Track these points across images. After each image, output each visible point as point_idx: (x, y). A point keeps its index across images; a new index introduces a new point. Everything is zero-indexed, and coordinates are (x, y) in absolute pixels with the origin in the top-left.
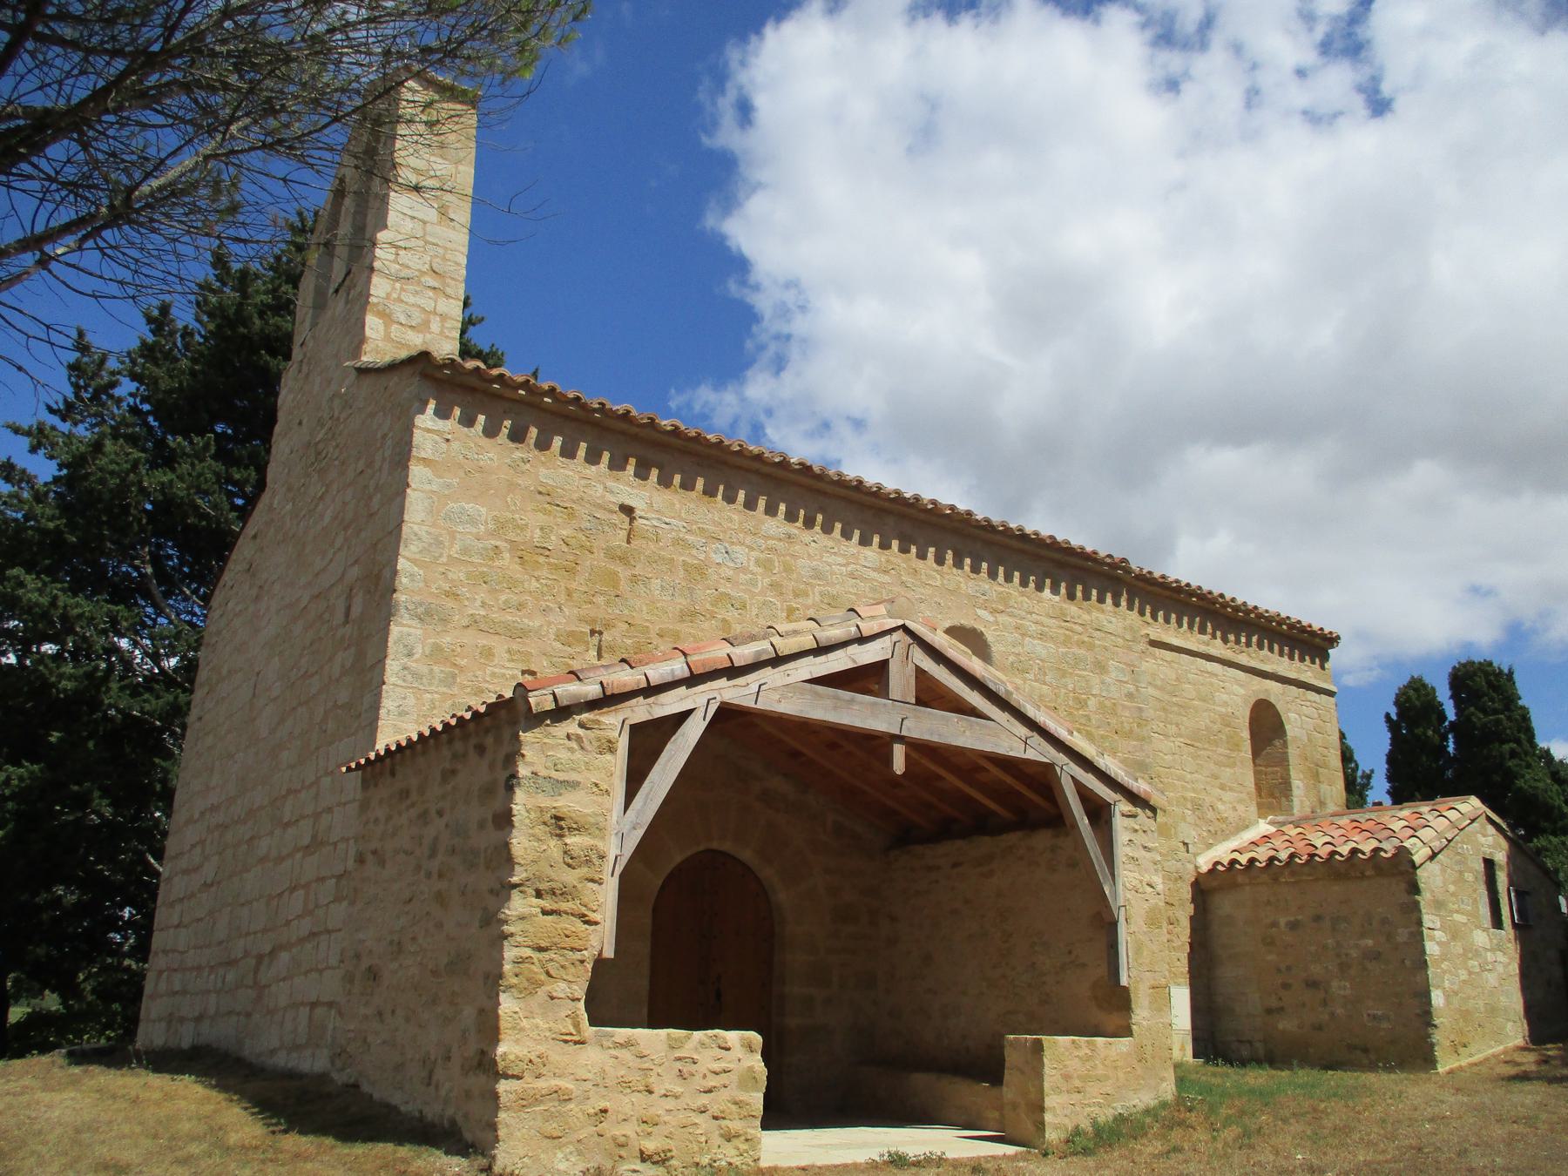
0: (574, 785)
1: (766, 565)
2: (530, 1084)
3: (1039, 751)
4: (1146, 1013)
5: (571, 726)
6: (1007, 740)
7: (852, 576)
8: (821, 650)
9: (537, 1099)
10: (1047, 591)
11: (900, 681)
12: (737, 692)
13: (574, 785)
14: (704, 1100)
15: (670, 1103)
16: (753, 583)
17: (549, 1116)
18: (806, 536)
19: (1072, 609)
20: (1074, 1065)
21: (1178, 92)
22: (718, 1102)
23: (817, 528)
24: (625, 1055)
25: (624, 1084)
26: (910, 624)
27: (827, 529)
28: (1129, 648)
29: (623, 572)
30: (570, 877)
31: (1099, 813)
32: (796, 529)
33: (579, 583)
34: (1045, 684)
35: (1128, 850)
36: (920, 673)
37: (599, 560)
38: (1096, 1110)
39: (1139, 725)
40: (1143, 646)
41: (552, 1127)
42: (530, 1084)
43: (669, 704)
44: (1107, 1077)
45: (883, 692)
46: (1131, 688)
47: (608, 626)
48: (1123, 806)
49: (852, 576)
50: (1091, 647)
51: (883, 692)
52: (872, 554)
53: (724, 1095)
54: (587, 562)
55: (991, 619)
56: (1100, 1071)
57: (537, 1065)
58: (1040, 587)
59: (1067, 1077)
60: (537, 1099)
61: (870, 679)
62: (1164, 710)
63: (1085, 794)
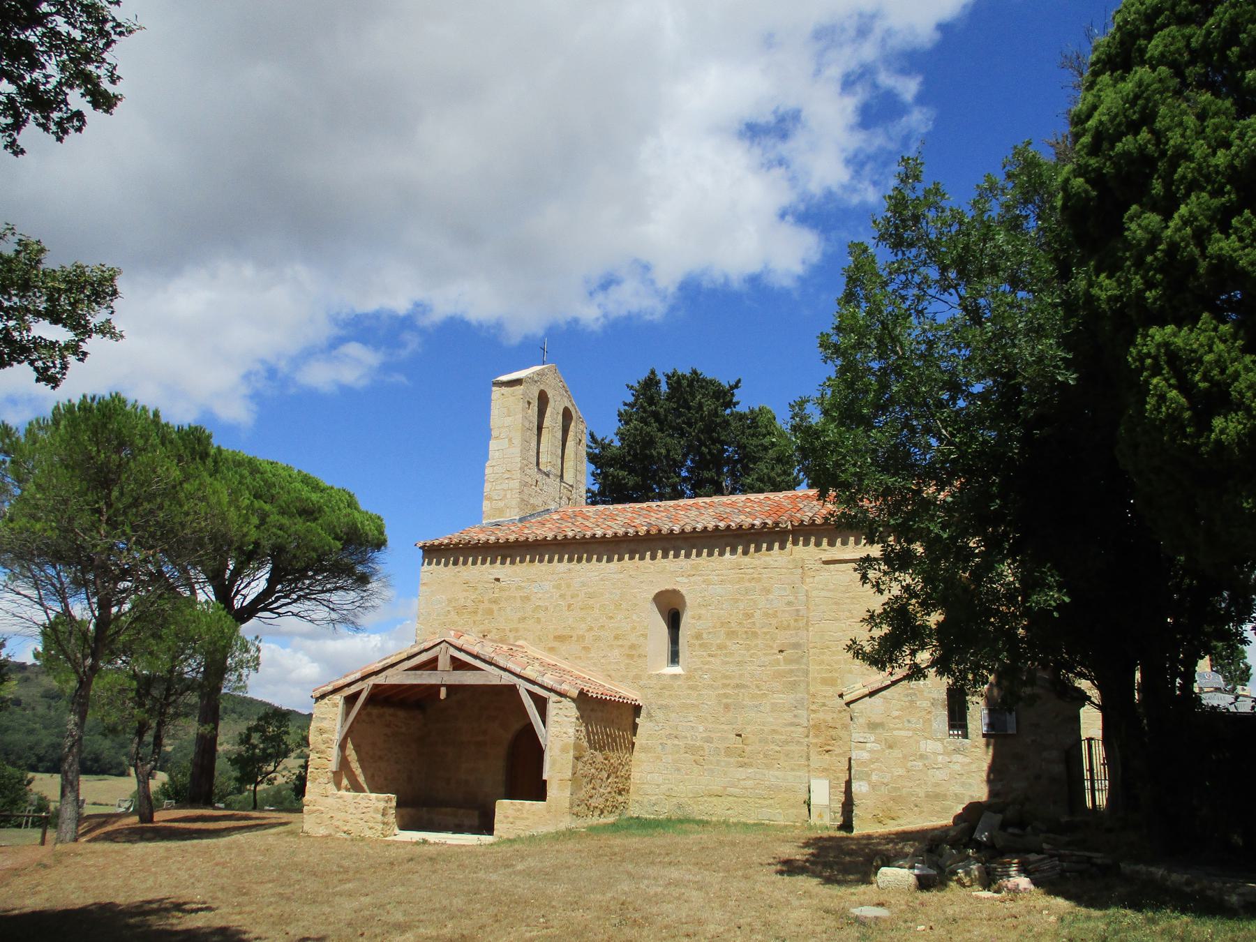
0: (325, 719)
1: (558, 587)
2: (311, 807)
3: (507, 679)
4: (555, 792)
5: (326, 700)
6: (493, 677)
7: (602, 580)
8: (409, 658)
9: (314, 812)
10: (727, 555)
11: (443, 663)
12: (379, 680)
13: (325, 719)
14: (362, 816)
15: (352, 816)
16: (551, 597)
17: (317, 817)
18: (579, 566)
19: (746, 560)
20: (510, 812)
21: (848, 162)
22: (366, 817)
23: (584, 561)
24: (340, 800)
25: (339, 809)
26: (447, 639)
27: (589, 560)
28: (792, 573)
29: (495, 607)
30: (323, 747)
31: (541, 704)
32: (574, 565)
33: (479, 618)
34: (722, 609)
35: (556, 719)
36: (453, 658)
37: (487, 605)
38: (520, 832)
39: (796, 621)
40: (819, 565)
41: (319, 821)
42: (311, 807)
43: (354, 689)
44: (528, 819)
45: (435, 668)
46: (791, 598)
47: (490, 632)
48: (553, 697)
49: (602, 580)
50: (759, 580)
51: (435, 668)
52: (615, 565)
53: (369, 815)
54: (481, 606)
55: (686, 581)
56: (525, 815)
57: (315, 803)
58: (722, 554)
59: (507, 817)
60: (314, 812)
61: (431, 665)
62: (836, 603)
63: (532, 695)
